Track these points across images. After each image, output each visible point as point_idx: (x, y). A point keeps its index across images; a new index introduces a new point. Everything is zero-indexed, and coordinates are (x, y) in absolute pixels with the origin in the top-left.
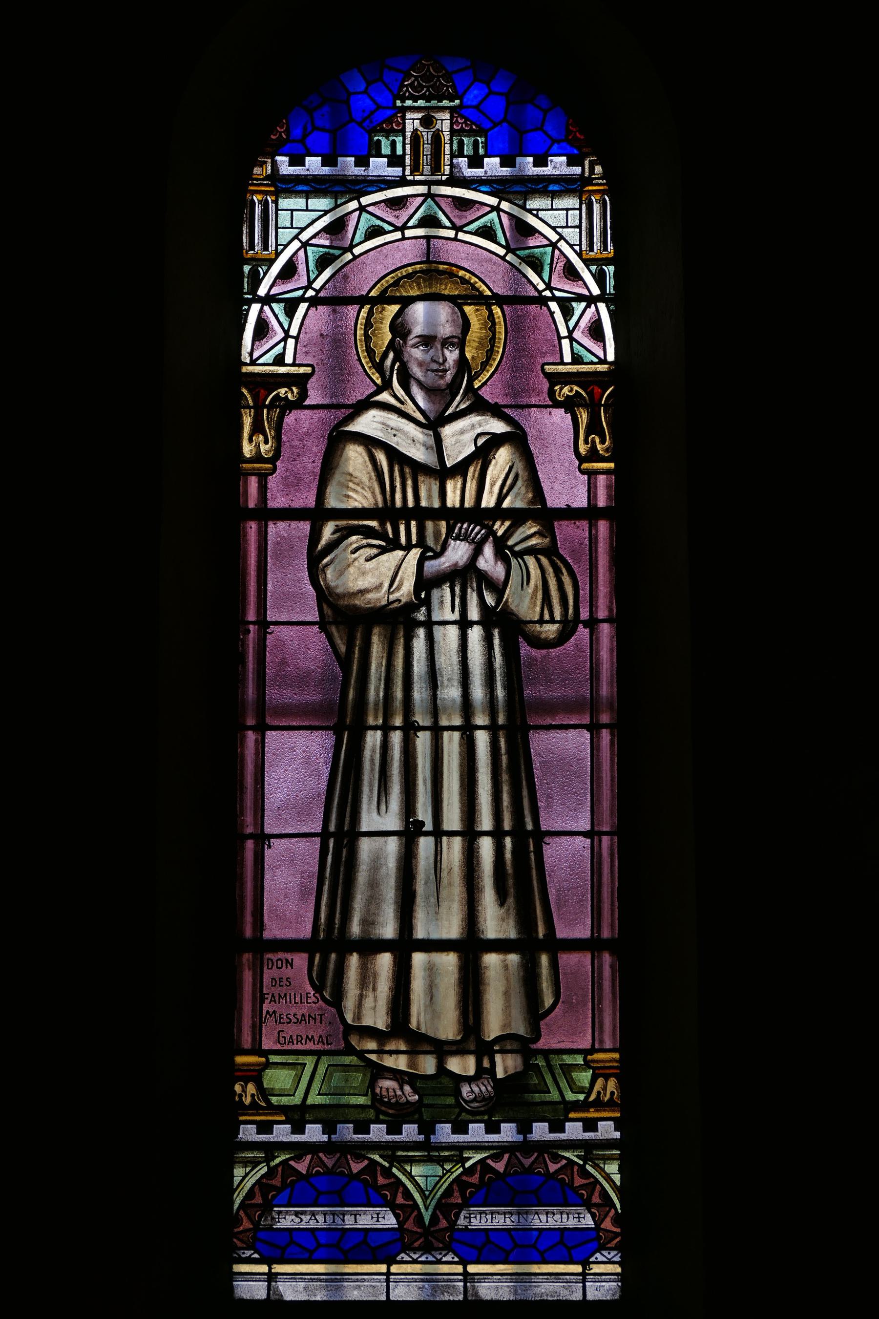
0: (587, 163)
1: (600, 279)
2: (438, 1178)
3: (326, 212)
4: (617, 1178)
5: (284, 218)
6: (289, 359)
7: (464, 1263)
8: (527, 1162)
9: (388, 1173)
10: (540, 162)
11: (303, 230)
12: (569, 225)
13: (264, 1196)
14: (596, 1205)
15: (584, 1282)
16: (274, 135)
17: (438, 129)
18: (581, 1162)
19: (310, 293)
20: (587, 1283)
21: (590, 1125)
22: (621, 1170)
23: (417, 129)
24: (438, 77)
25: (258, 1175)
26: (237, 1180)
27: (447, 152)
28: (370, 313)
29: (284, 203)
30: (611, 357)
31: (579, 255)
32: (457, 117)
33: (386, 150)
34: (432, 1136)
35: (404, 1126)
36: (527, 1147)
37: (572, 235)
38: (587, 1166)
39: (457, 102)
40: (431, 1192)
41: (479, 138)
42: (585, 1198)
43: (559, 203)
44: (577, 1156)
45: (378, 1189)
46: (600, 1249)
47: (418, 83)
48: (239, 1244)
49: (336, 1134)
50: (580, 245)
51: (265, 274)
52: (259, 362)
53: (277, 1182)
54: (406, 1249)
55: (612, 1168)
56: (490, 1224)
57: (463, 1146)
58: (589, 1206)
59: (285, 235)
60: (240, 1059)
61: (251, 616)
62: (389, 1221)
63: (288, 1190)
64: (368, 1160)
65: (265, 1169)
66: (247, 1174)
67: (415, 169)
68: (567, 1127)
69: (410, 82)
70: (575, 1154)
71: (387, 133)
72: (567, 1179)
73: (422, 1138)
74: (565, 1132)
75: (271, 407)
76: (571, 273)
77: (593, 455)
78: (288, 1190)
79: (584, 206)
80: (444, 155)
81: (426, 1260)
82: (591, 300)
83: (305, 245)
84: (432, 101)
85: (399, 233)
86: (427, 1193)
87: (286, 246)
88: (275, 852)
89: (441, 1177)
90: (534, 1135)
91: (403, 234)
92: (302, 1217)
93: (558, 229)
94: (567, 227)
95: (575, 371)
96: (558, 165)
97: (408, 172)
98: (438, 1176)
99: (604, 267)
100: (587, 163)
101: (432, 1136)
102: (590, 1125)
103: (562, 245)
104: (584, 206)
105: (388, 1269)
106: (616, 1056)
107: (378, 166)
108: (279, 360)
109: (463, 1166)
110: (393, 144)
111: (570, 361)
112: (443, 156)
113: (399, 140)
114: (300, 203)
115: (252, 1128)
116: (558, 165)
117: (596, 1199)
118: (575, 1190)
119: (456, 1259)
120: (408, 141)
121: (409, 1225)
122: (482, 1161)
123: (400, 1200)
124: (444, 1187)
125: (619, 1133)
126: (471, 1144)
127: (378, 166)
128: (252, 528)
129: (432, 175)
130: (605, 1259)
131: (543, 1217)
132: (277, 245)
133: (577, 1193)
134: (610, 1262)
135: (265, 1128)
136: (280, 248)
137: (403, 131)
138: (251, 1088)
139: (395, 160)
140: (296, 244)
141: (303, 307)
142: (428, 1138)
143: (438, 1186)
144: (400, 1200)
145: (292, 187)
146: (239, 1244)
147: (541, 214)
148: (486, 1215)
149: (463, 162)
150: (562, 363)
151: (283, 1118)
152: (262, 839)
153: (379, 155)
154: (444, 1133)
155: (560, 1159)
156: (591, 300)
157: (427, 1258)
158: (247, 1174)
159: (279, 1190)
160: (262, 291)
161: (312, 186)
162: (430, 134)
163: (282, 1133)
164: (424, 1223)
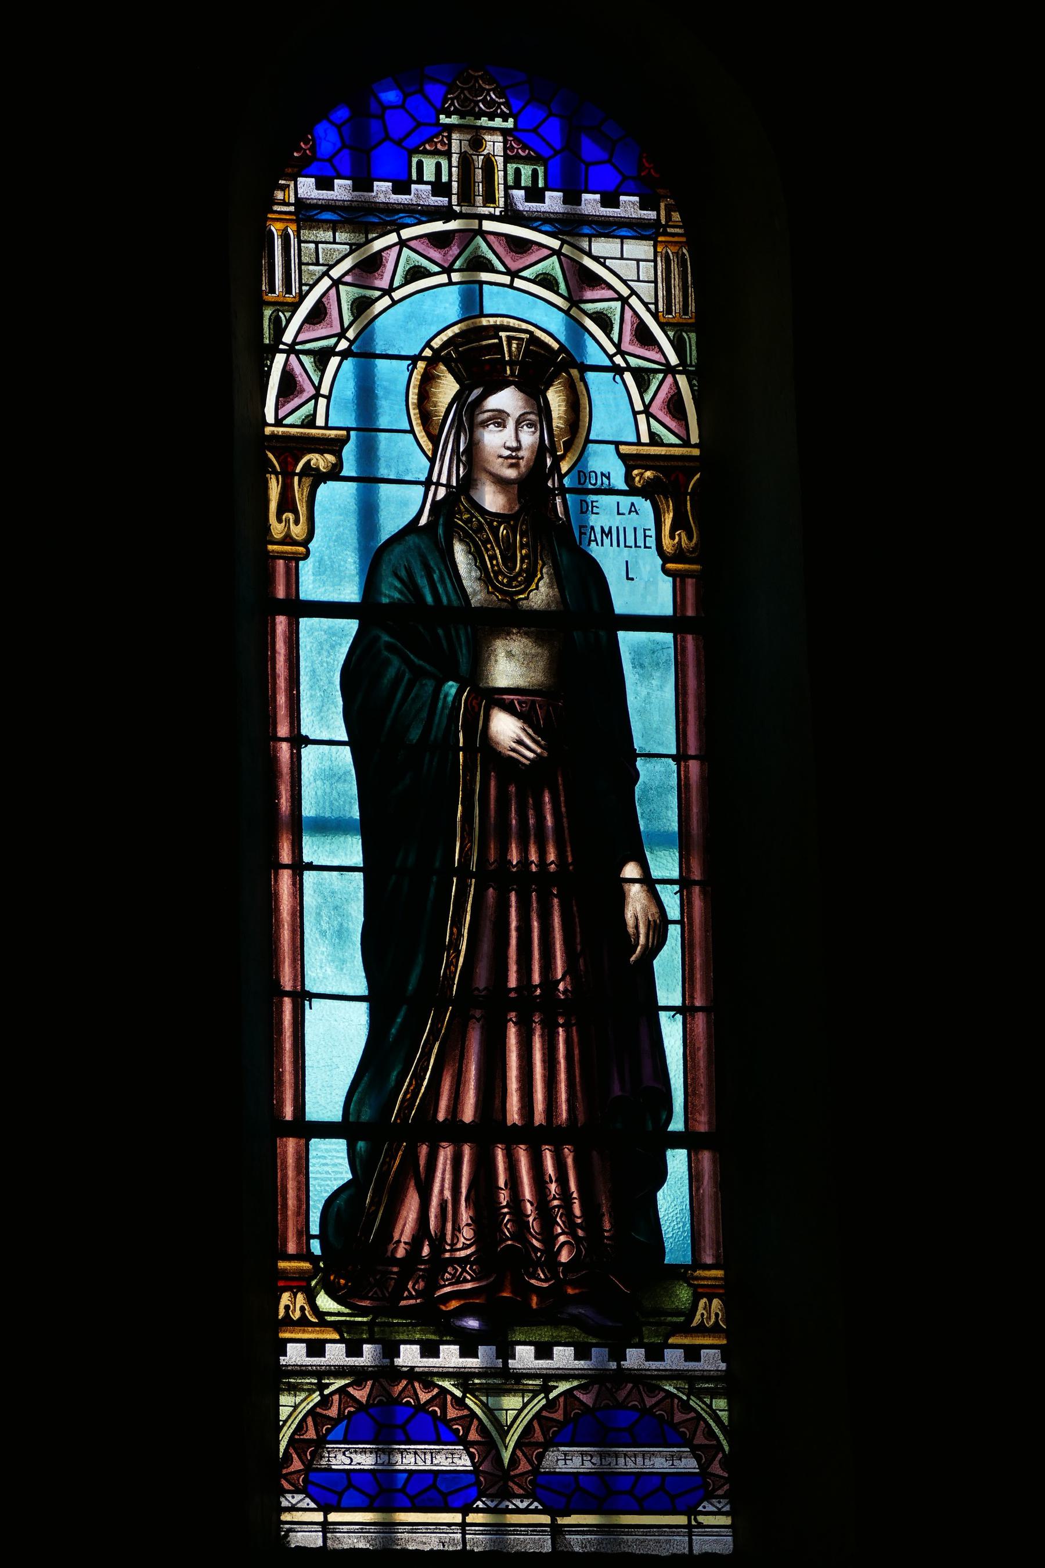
1: (679, 347)
4: (724, 1415)
6: (320, 421)
7: (325, 1508)
9: (460, 1403)
10: (610, 200)
11: (331, 267)
14: (473, 1443)
15: (690, 1535)
17: (489, 153)
18: (458, 1393)
19: (343, 345)
20: (467, 1536)
21: (692, 1353)
22: (730, 1410)
24: (488, 91)
26: (284, 1413)
29: (305, 234)
30: (695, 439)
31: (655, 315)
33: (429, 175)
34: (281, 1358)
37: (646, 290)
38: (691, 1401)
39: (510, 124)
41: (423, 160)
46: (709, 1496)
48: (286, 1486)
50: (656, 304)
51: (288, 321)
52: (287, 421)
53: (559, 1416)
55: (720, 1404)
57: (522, 1373)
58: (467, 1445)
60: (282, 1264)
61: (283, 731)
62: (689, 1464)
64: (438, 1388)
66: (525, 1405)
67: (466, 197)
72: (577, 1411)
74: (362, 1357)
75: (301, 475)
76: (644, 336)
77: (679, 555)
82: (669, 370)
83: (336, 283)
84: (482, 118)
85: (509, 278)
87: (312, 287)
88: (316, 1014)
89: (521, 1411)
90: (628, 1361)
91: (512, 281)
92: (352, 1456)
94: (638, 280)
95: (635, 452)
96: (629, 206)
100: (662, 205)
101: (281, 1358)
102: (692, 1353)
103: (634, 301)
105: (464, 1519)
106: (720, 1273)
107: (421, 194)
108: (310, 422)
110: (438, 166)
114: (328, 235)
115: (302, 1348)
117: (473, 1436)
118: (675, 1427)
120: (455, 163)
123: (473, 1436)
126: (560, 1372)
128: (281, 623)
130: (715, 1509)
131: (340, 1456)
132: (301, 284)
133: (450, 1428)
134: (719, 1513)
135: (316, 1348)
136: (305, 288)
137: (448, 154)
138: (300, 1299)
139: (440, 188)
140: (326, 282)
141: (335, 361)
144: (700, 1440)
146: (286, 1486)
147: (608, 262)
148: (592, 1457)
149: (519, 194)
150: (639, 443)
152: (302, 997)
153: (420, 181)
154: (524, 1357)
155: (657, 1392)
157: (308, 1504)
158: (525, 1405)
160: (288, 337)
163: (336, 1354)
164: (503, 1464)
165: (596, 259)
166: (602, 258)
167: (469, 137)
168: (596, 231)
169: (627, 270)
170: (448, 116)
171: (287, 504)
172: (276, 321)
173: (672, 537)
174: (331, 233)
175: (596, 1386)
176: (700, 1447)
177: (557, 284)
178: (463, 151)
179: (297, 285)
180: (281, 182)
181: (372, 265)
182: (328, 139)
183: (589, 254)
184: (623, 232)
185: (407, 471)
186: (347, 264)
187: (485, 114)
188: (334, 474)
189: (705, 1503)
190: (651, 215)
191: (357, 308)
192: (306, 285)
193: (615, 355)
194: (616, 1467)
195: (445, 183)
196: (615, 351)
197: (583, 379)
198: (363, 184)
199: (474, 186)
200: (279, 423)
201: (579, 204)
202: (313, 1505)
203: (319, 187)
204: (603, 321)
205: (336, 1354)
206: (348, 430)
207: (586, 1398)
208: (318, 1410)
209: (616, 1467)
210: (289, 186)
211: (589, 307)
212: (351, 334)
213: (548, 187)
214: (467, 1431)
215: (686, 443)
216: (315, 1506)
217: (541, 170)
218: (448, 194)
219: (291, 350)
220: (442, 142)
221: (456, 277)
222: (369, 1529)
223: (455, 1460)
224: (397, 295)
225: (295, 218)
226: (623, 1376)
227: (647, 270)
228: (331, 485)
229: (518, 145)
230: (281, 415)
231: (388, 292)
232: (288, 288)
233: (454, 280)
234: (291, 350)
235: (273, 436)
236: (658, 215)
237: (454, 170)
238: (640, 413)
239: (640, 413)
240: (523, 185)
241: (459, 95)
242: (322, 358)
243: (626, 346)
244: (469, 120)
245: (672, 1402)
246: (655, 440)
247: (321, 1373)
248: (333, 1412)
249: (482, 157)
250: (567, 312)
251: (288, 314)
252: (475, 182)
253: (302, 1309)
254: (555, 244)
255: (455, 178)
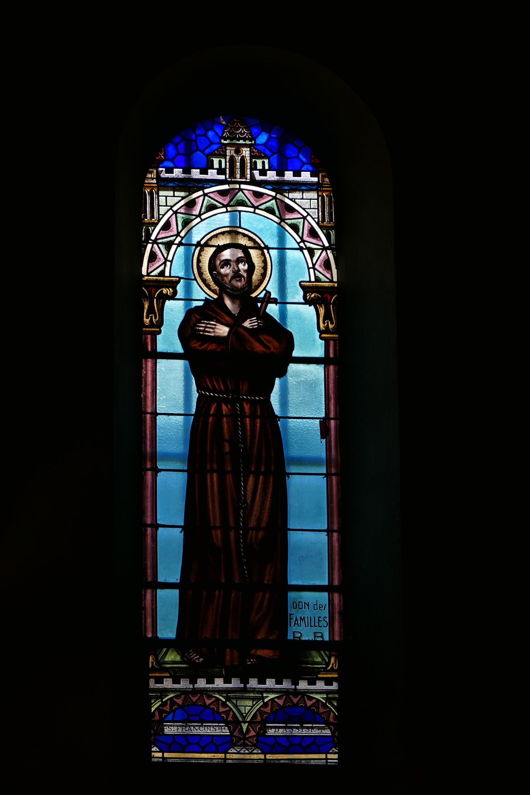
0: (320, 176)
2: (250, 707)
3: (183, 198)
5: (162, 200)
6: (167, 274)
8: (295, 700)
9: (224, 705)
10: (297, 174)
12: (312, 208)
13: (160, 715)
16: (158, 157)
18: (224, 700)
23: (233, 155)
25: (258, 707)
27: (249, 167)
28: (200, 251)
29: (161, 193)
30: (335, 279)
31: (318, 223)
32: (253, 149)
33: (216, 165)
35: (164, 679)
36: (195, 691)
40: (247, 714)
42: (153, 719)
43: (306, 195)
44: (323, 698)
45: (319, 714)
47: (248, 137)
49: (299, 685)
51: (153, 231)
52: (152, 274)
53: (167, 709)
54: (233, 746)
56: (311, 732)
58: (227, 723)
59: (163, 210)
62: (226, 732)
63: (172, 714)
65: (160, 703)
68: (232, 681)
69: (228, 130)
70: (322, 696)
71: (217, 156)
73: (242, 686)
76: (313, 233)
77: (328, 330)
78: (172, 714)
79: (320, 198)
80: (247, 169)
81: (244, 752)
82: (324, 248)
83: (176, 213)
86: (245, 715)
87: (164, 215)
89: (252, 707)
93: (306, 210)
96: (306, 176)
97: (227, 177)
98: (251, 706)
99: (330, 231)
100: (320, 175)
103: (309, 218)
104: (320, 198)
107: (212, 174)
108: (162, 273)
109: (263, 701)
110: (220, 162)
111: (314, 280)
112: (246, 169)
113: (223, 161)
114: (171, 193)
116: (306, 176)
117: (230, 719)
119: (260, 752)
120: (227, 160)
121: (236, 733)
122: (272, 700)
124: (253, 713)
125: (243, 685)
127: (212, 174)
129: (240, 179)
130: (236, 752)
132: (159, 215)
137: (225, 156)
139: (221, 171)
140: (171, 212)
141: (174, 247)
142: (245, 686)
143: (251, 711)
145: (298, 188)
149: (256, 173)
151: (168, 675)
152: (156, 526)
153: (213, 168)
156: (324, 248)
158: (253, 705)
159: (168, 713)
160: (153, 237)
161: (289, 187)
162: (240, 158)
163: (168, 683)
165: (291, 200)
166: (293, 199)
167: (234, 149)
168: (290, 187)
169: (305, 204)
170: (225, 140)
171: (151, 310)
172: (147, 231)
173: (324, 323)
174: (172, 192)
175: (284, 697)
176: (230, 722)
177: (215, 205)
178: (231, 155)
179: (157, 215)
180: (151, 170)
181: (191, 204)
182: (171, 150)
183: (288, 198)
184: (303, 188)
185: (199, 296)
186: (182, 203)
187: (242, 139)
188: (173, 297)
189: (334, 749)
190: (315, 179)
191: (184, 224)
192: (161, 215)
193: (300, 242)
194: (302, 732)
195: (223, 168)
196: (300, 240)
197: (268, 252)
198: (187, 171)
199: (236, 170)
200: (148, 274)
201: (284, 176)
202: (158, 750)
203: (201, 173)
204: (295, 228)
205: (168, 683)
206: (180, 278)
207: (281, 702)
208: (161, 708)
209: (302, 732)
210: (153, 171)
211: (289, 222)
212: (182, 234)
213: (270, 169)
214: (227, 717)
215: (331, 281)
216: (159, 750)
217: (266, 161)
218: (225, 174)
219: (155, 242)
220: (222, 151)
221: (229, 209)
222: (201, 761)
223: (222, 730)
224: (203, 217)
225: (157, 185)
226: (296, 693)
227: (314, 203)
228: (172, 302)
229: (256, 150)
230: (150, 270)
231: (199, 215)
232: (152, 217)
233: (229, 210)
234: (155, 242)
235: (147, 280)
236: (319, 179)
237: (228, 163)
238: (311, 268)
239: (311, 268)
240: (258, 168)
241: (230, 130)
242: (168, 245)
243: (305, 238)
244: (235, 141)
245: (318, 705)
246: (317, 279)
247: (262, 692)
248: (221, 710)
249: (240, 157)
250: (279, 224)
251: (153, 228)
252: (236, 168)
253: (153, 663)
254: (273, 194)
255: (228, 167)
